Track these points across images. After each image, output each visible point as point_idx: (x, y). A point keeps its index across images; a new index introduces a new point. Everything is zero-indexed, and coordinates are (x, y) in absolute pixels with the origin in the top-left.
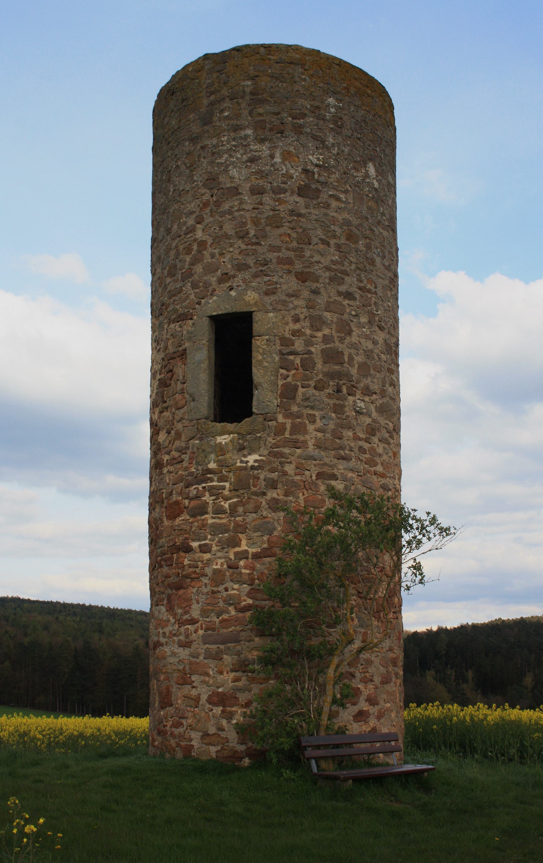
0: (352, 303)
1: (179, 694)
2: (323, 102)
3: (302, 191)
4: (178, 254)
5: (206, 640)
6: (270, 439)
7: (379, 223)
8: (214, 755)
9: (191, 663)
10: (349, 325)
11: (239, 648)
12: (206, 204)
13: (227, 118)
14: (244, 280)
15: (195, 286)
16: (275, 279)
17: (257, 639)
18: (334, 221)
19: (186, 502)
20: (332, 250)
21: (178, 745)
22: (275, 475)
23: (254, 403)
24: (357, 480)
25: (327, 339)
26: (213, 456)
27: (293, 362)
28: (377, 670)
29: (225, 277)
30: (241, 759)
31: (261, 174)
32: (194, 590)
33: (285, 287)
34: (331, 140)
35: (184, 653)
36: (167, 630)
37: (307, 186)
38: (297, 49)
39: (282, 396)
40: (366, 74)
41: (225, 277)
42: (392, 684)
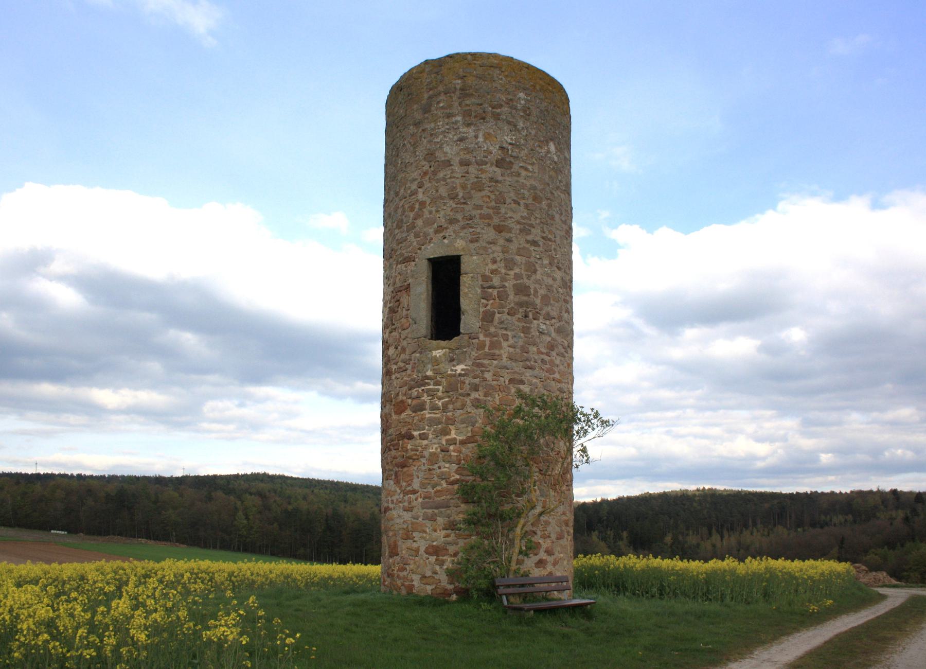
0: (536, 249)
1: (404, 547)
2: (515, 96)
3: (499, 163)
6: (473, 353)
7: (558, 188)
8: (430, 593)
9: (412, 523)
11: (449, 512)
12: (425, 173)
13: (442, 108)
14: (454, 232)
15: (417, 236)
17: (463, 505)
19: (410, 401)
20: (522, 208)
21: (403, 585)
22: (477, 381)
23: (462, 325)
25: (517, 277)
28: (553, 529)
30: (450, 595)
31: (468, 150)
35: (407, 516)
39: (483, 320)
40: (548, 75)
41: (440, 229)
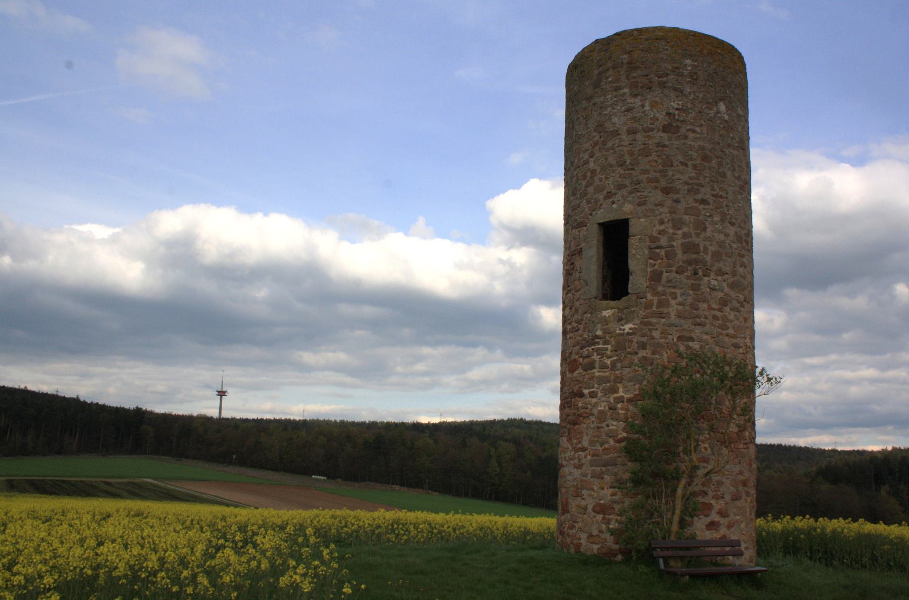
0: (706, 207)
1: (574, 503)
3: (665, 129)
4: (577, 180)
5: (592, 464)
6: (641, 312)
7: (729, 146)
8: (596, 552)
9: (581, 481)
10: (704, 223)
11: (616, 470)
12: (596, 144)
13: (610, 82)
14: (623, 196)
15: (588, 202)
16: (646, 194)
17: (629, 464)
18: (691, 148)
19: (581, 360)
20: (690, 169)
21: (572, 543)
22: (644, 339)
23: (630, 286)
24: (711, 341)
25: (685, 235)
26: (599, 326)
27: (658, 254)
28: (728, 489)
29: (610, 195)
30: (615, 555)
32: (585, 426)
33: (652, 199)
34: (688, 90)
35: (577, 473)
36: (567, 455)
37: (670, 125)
38: (660, 29)
39: (651, 279)
40: (717, 39)
41: (610, 195)
42: (742, 501)
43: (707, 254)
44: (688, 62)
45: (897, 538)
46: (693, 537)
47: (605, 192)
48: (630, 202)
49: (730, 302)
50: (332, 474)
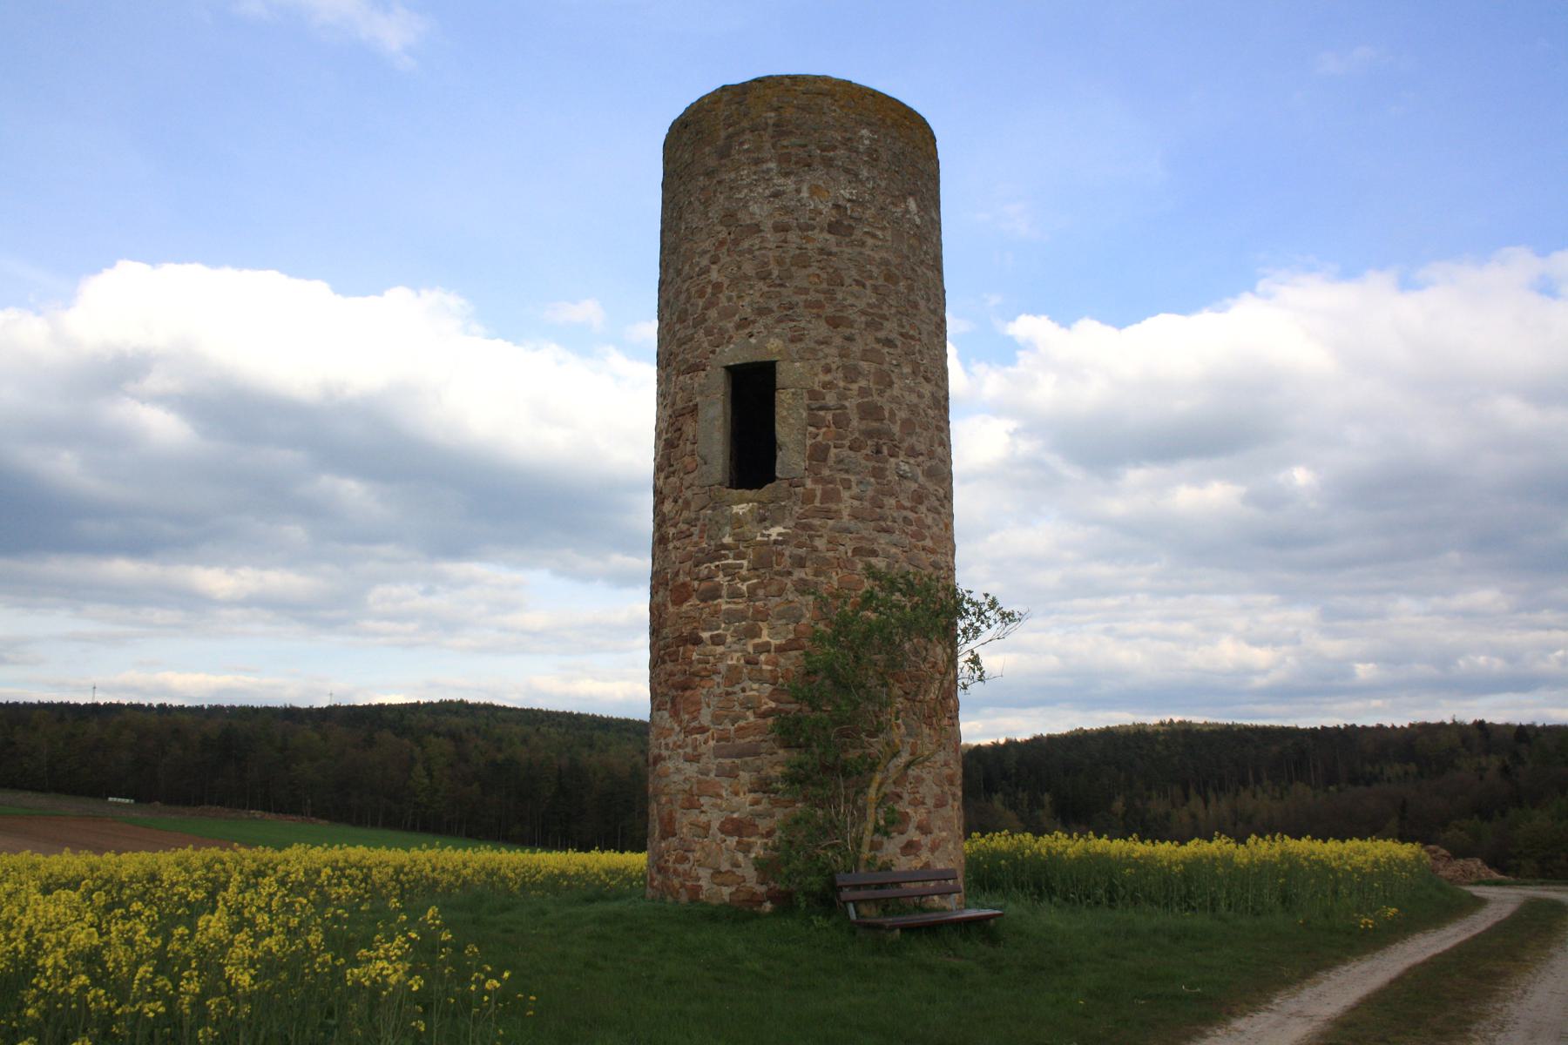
1: (684, 821)
3: (833, 228)
4: (689, 299)
5: (718, 753)
6: (796, 509)
7: (922, 262)
8: (727, 899)
9: (699, 782)
11: (758, 762)
12: (722, 243)
13: (748, 151)
15: (708, 333)
17: (781, 752)
18: (870, 260)
19: (696, 583)
20: (868, 292)
21: (683, 886)
23: (778, 466)
24: (902, 557)
25: (863, 392)
26: (728, 529)
27: (823, 419)
28: (929, 790)
29: (744, 323)
30: (760, 903)
33: (813, 333)
34: (865, 174)
35: (691, 769)
36: (670, 740)
38: (826, 79)
39: (811, 457)
43: (894, 423)
44: (865, 132)
45: (1141, 857)
46: (886, 867)
47: (737, 318)
48: (778, 336)
49: (927, 497)
50: (143, 795)
